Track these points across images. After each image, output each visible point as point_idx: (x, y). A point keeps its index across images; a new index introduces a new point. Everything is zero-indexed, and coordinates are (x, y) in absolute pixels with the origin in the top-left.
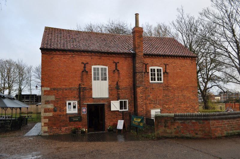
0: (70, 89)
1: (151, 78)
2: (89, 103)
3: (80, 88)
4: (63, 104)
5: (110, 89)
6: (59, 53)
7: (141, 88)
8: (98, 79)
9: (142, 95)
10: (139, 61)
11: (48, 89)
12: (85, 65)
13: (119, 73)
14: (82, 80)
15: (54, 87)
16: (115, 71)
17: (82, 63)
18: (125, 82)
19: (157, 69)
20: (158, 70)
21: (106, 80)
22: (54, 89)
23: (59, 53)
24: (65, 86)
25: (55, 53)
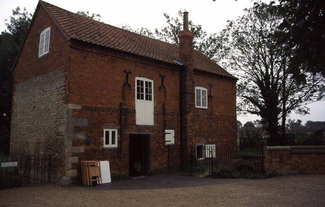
0: (109, 109)
1: (137, 94)
2: (132, 133)
3: (121, 110)
4: (99, 133)
5: (156, 113)
6: (96, 51)
7: (191, 114)
8: (142, 98)
9: (191, 124)
10: (189, 78)
11: (79, 107)
12: (128, 74)
13: (165, 92)
14: (123, 97)
15: (87, 105)
16: (161, 88)
17: (124, 71)
18: (173, 105)
19: (146, 82)
20: (146, 82)
21: (150, 100)
22: (87, 108)
23: (96, 51)
24: (102, 104)
25: (90, 50)
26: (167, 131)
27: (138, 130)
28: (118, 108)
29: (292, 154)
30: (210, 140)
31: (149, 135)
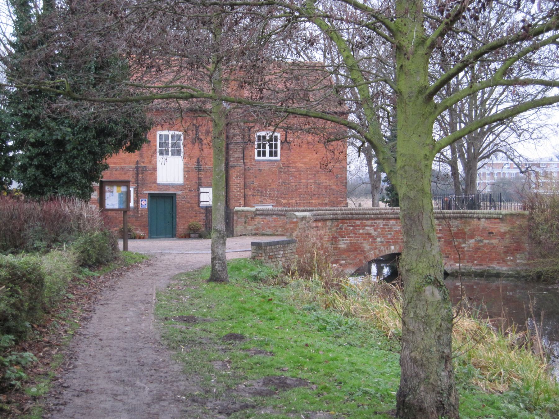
3: (137, 168)
5: (186, 169)
21: (179, 154)
26: (202, 190)
27: (160, 190)
28: (134, 166)
29: (256, 215)
30: (284, 201)
31: (175, 194)
